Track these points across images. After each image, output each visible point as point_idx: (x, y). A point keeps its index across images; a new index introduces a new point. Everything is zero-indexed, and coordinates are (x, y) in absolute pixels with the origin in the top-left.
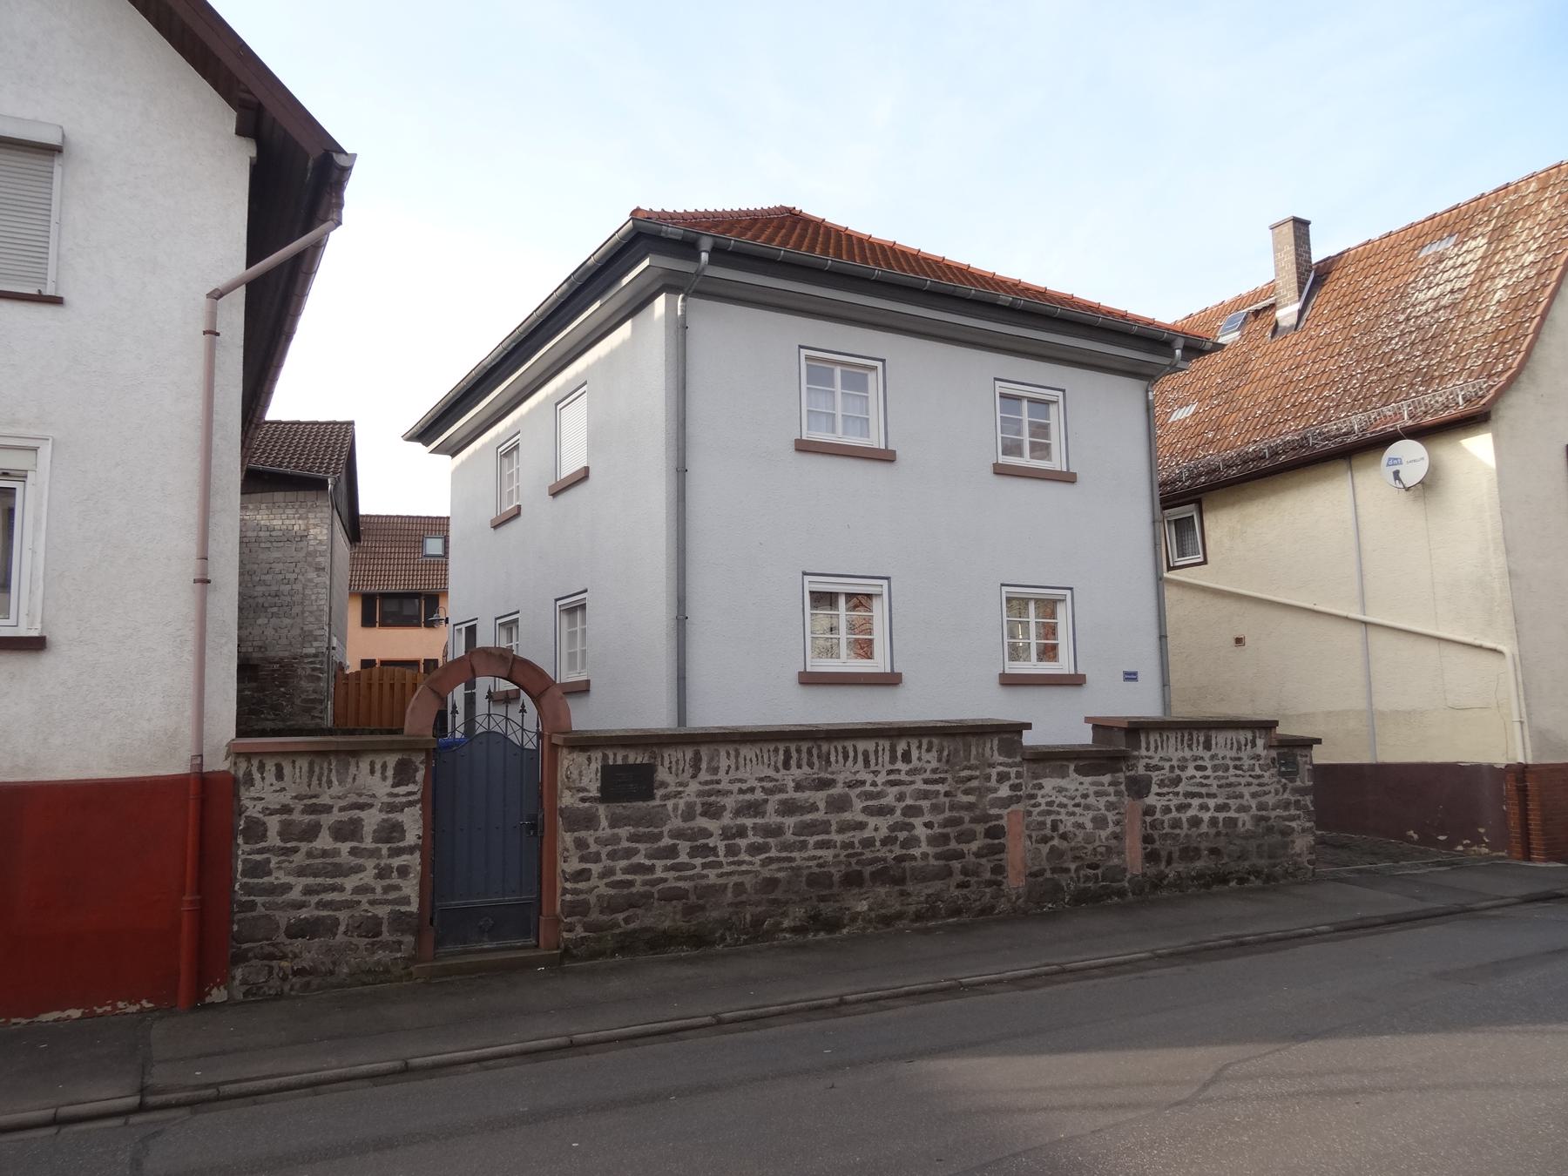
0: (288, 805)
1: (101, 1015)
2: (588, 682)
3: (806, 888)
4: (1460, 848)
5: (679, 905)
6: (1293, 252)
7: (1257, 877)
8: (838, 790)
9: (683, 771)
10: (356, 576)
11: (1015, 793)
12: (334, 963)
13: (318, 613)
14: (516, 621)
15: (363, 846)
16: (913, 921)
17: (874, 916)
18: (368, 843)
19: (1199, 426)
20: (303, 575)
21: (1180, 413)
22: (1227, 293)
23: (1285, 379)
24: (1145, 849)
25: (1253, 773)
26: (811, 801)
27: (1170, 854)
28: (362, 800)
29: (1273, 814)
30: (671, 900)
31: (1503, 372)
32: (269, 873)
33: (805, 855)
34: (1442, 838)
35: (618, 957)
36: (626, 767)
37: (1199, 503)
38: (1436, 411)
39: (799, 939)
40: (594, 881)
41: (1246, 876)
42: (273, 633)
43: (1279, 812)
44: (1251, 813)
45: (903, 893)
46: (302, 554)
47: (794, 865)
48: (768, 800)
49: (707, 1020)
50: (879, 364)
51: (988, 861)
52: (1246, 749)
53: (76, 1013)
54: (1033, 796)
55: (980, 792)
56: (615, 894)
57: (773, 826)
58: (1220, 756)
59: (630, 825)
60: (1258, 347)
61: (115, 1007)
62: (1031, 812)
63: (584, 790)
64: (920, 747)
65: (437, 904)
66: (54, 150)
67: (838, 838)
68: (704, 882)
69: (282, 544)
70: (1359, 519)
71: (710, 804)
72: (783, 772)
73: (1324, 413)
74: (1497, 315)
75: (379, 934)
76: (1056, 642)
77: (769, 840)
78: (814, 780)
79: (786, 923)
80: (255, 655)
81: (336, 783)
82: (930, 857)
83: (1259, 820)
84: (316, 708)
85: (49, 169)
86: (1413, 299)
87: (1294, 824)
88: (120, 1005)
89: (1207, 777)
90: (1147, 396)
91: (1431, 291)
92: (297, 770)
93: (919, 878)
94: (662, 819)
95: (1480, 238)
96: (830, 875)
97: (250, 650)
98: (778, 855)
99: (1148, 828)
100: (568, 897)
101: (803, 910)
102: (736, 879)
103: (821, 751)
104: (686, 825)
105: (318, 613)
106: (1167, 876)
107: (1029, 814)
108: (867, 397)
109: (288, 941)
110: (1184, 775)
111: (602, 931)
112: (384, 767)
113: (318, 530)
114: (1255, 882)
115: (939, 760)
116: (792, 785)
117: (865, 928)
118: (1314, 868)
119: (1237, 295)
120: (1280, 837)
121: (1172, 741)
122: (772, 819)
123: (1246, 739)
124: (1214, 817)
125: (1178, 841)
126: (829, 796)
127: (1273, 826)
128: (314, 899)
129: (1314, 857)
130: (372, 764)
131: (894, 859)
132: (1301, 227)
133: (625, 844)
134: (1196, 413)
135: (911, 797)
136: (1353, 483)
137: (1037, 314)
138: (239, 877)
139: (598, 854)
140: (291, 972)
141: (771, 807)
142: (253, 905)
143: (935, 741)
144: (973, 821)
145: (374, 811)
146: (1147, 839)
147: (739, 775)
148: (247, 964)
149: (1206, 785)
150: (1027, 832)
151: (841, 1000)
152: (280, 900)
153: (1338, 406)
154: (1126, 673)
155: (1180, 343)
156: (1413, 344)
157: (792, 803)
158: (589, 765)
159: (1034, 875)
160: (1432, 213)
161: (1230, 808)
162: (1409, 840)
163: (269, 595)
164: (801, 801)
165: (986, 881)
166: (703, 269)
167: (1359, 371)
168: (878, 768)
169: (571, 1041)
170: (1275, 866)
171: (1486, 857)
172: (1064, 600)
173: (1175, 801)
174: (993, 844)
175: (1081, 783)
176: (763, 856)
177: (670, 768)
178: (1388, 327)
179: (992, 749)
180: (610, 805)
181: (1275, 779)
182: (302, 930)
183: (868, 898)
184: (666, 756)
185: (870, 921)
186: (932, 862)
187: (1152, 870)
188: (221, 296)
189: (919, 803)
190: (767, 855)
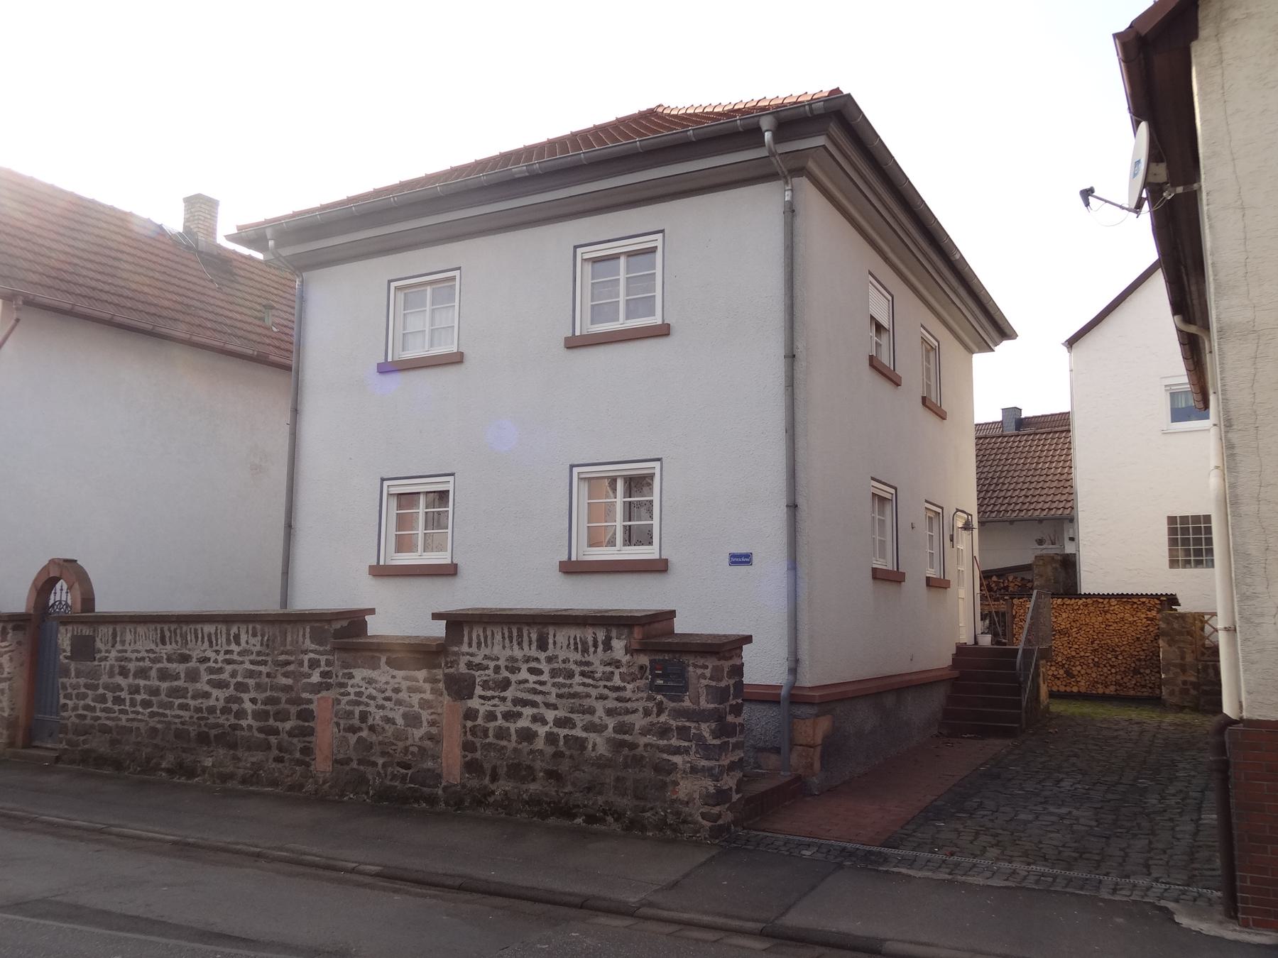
5: (108, 736)
7: (616, 820)
8: (193, 664)
11: (325, 680)
24: (465, 756)
25: (608, 684)
27: (494, 768)
43: (649, 739)
47: (166, 719)
58: (560, 659)
67: (192, 703)
72: (161, 646)
77: (153, 698)
79: (164, 765)
83: (618, 745)
87: (677, 759)
89: (542, 683)
96: (188, 732)
106: (493, 792)
107: (339, 702)
110: (513, 678)
115: (262, 645)
121: (498, 637)
125: (504, 754)
127: (642, 757)
143: (258, 627)
144: (288, 701)
146: (468, 747)
149: (541, 693)
150: (335, 720)
159: (336, 761)
170: (644, 811)
174: (304, 726)
175: (393, 677)
181: (644, 695)
187: (474, 783)
189: (247, 680)
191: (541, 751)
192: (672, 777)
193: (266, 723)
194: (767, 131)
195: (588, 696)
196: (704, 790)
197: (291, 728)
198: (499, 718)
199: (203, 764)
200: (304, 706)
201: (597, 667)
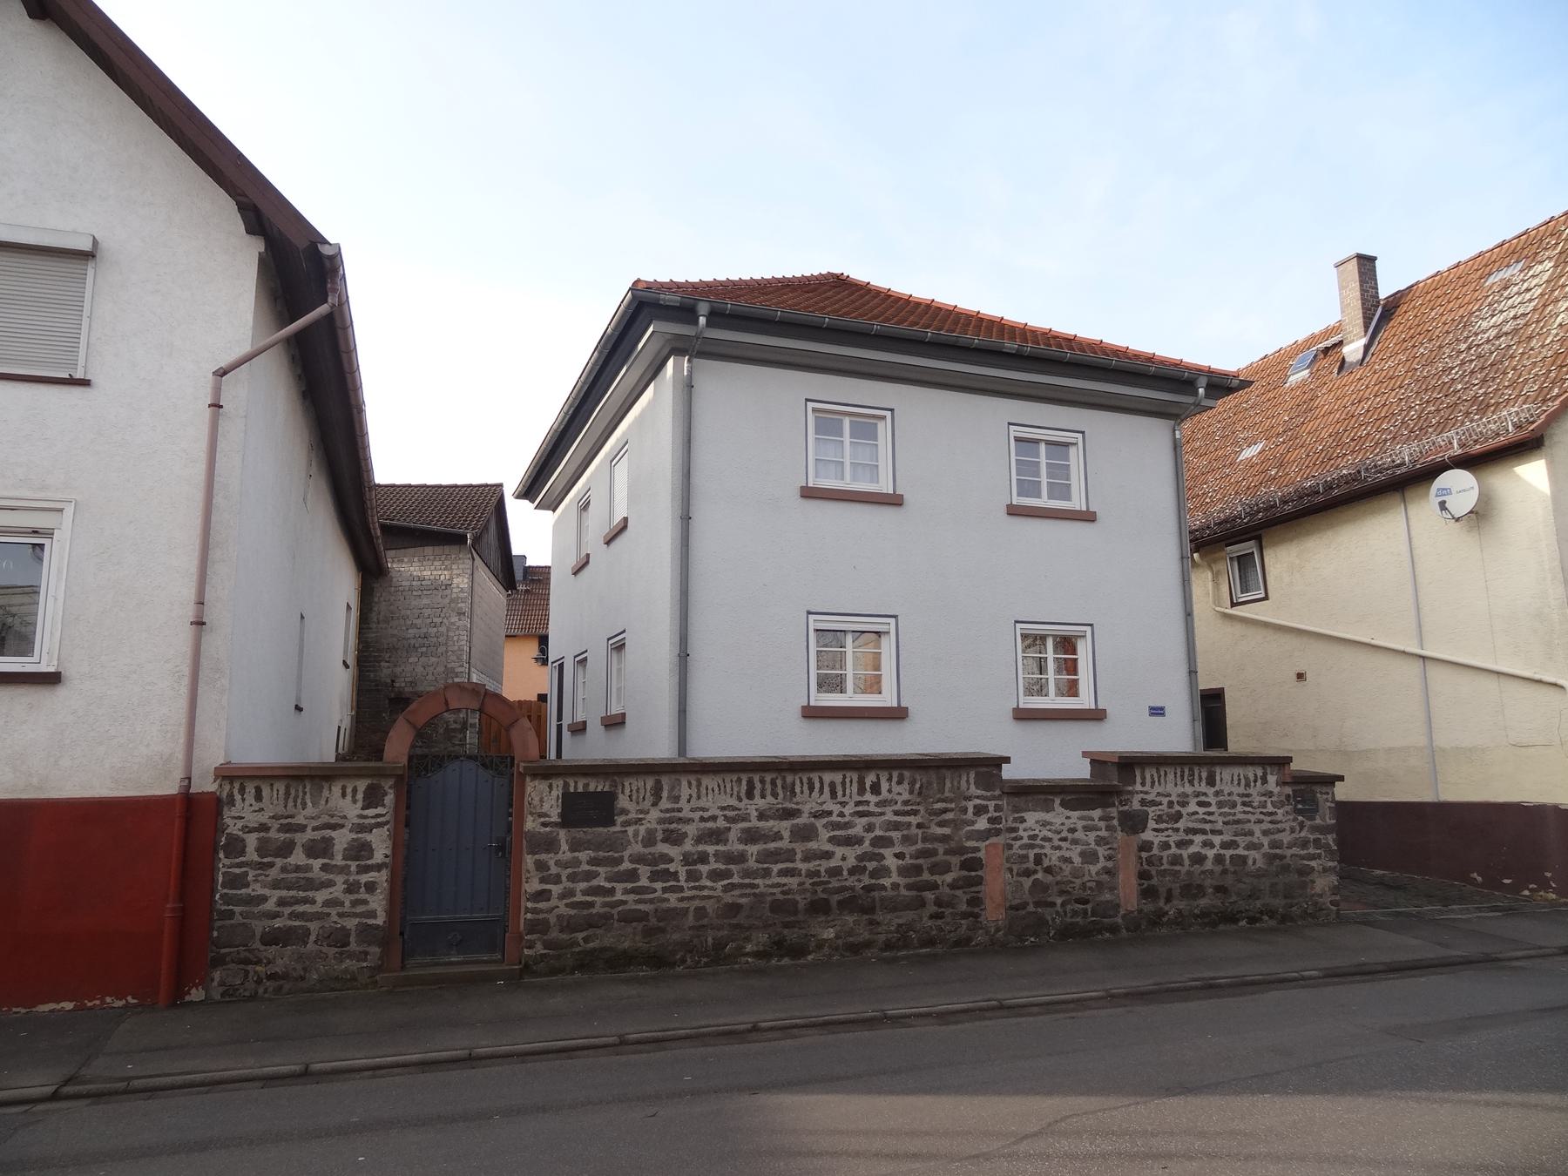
0: (265, 824)
1: (91, 1008)
3: (769, 914)
4: (1526, 893)
5: (639, 926)
6: (1358, 288)
7: (1271, 917)
8: (803, 820)
9: (644, 798)
12: (305, 969)
15: (334, 863)
16: (882, 950)
17: (841, 944)
18: (338, 860)
21: (1248, 452)
25: (1264, 811)
26: (775, 830)
27: (1169, 891)
28: (333, 821)
29: (1289, 852)
30: (632, 922)
31: (1558, 396)
32: (247, 885)
33: (768, 882)
34: (1507, 881)
35: (577, 975)
36: (586, 795)
37: (1259, 539)
38: (1487, 440)
39: (762, 963)
40: (554, 902)
41: (1258, 915)
43: (1295, 850)
44: (1263, 851)
45: (871, 923)
46: (447, 600)
47: (757, 891)
48: (730, 828)
49: (611, 1040)
50: (888, 414)
52: (1255, 786)
53: (69, 1006)
54: (1015, 830)
55: (956, 824)
56: (575, 914)
58: (1226, 793)
61: (103, 1002)
62: (1012, 845)
63: (546, 815)
64: (890, 780)
65: (408, 918)
66: (88, 256)
67: (803, 867)
68: (665, 905)
69: (429, 592)
70: (1414, 552)
71: (672, 831)
72: (746, 801)
73: (1381, 445)
74: (1558, 338)
75: (348, 944)
76: (879, 673)
78: (778, 810)
79: (749, 948)
80: (407, 689)
81: (309, 804)
82: (902, 888)
83: (1271, 858)
84: (456, 737)
85: (84, 272)
86: (1476, 327)
87: (1313, 863)
88: (108, 1000)
90: (1174, 434)
91: (1495, 318)
92: (275, 792)
94: (622, 844)
95: (1547, 261)
96: (795, 903)
97: (403, 685)
98: (741, 881)
100: (529, 916)
102: (697, 903)
103: (785, 781)
104: (647, 851)
106: (1167, 913)
107: (1010, 847)
108: (877, 445)
109: (262, 948)
110: (1184, 811)
111: (562, 949)
112: (355, 791)
113: (460, 580)
115: (911, 792)
117: (831, 956)
118: (1338, 910)
120: (1296, 876)
121: (1171, 776)
126: (793, 825)
128: (287, 910)
130: (344, 789)
131: (862, 888)
132: (1366, 263)
133: (586, 867)
134: (1263, 451)
136: (1406, 513)
138: (219, 888)
139: (558, 876)
140: (264, 977)
141: (733, 835)
142: (231, 914)
143: (907, 774)
145: (344, 831)
146: (1143, 875)
147: (701, 803)
148: (224, 967)
149: (1210, 822)
150: (1008, 865)
151: (754, 1027)
152: (256, 910)
153: (1394, 438)
154: (1151, 708)
155: (1203, 381)
156: (1472, 372)
157: (755, 832)
159: (1012, 908)
160: (1500, 241)
161: (1238, 846)
162: (1473, 882)
164: (764, 830)
166: (701, 332)
167: (1418, 402)
168: (846, 799)
169: (470, 1054)
171: (1552, 903)
172: (1084, 636)
173: (1175, 838)
175: (1068, 818)
176: (726, 882)
178: (1450, 356)
179: (968, 783)
181: (1291, 817)
182: (275, 938)
184: (627, 784)
185: (837, 949)
186: (904, 892)
187: (1149, 907)
188: (225, 373)
190: (729, 881)
192: (1310, 877)
193: (920, 878)
195: (1249, 821)
199: (819, 938)
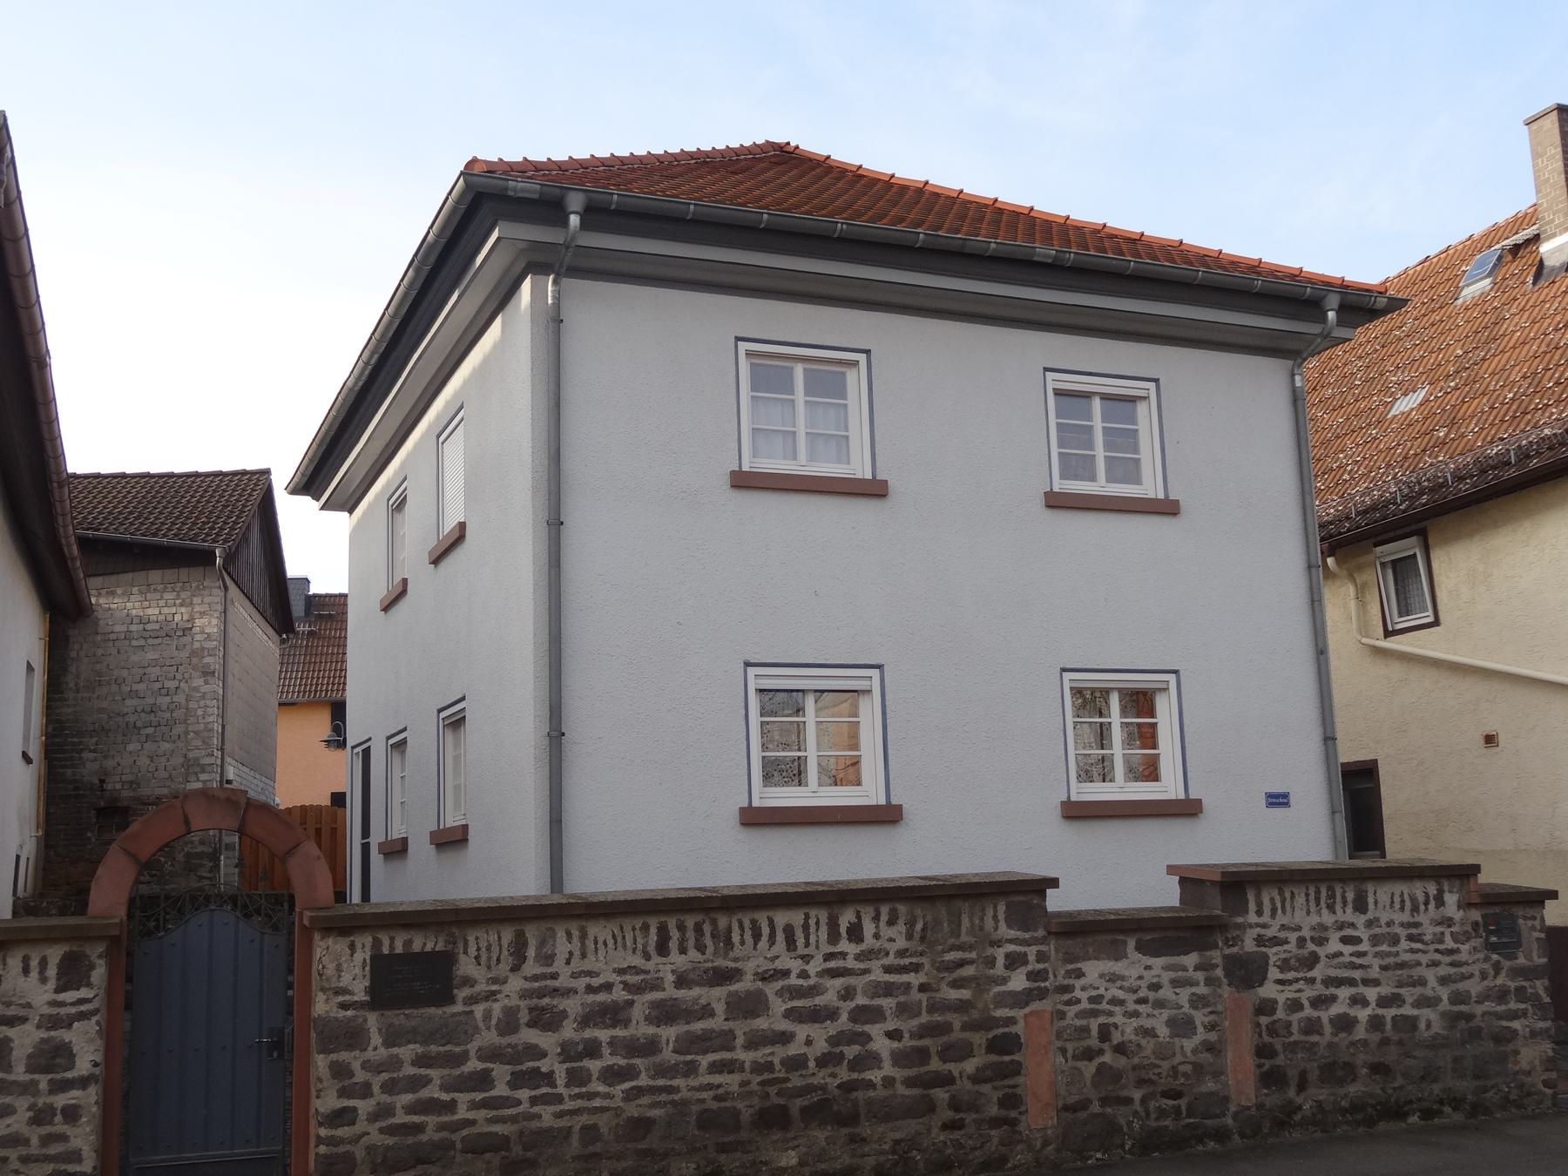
2: (465, 828)
5: (495, 1159)
7: (1455, 1109)
9: (498, 960)
10: (323, 678)
11: (1037, 984)
13: (206, 734)
14: (404, 741)
18: (19, 1073)
19: (1429, 421)
20: (186, 682)
22: (1477, 224)
23: (1548, 346)
24: (1260, 1066)
26: (703, 1002)
29: (1479, 1010)
30: (483, 1153)
36: (409, 958)
37: (1423, 534)
40: (361, 1126)
42: (148, 763)
43: (1489, 1006)
46: (185, 654)
47: (676, 1097)
50: (862, 358)
51: (995, 1088)
54: (1068, 989)
55: (980, 984)
57: (642, 1040)
58: (1383, 922)
59: (415, 1043)
60: (1515, 299)
64: (876, 918)
68: (535, 1125)
71: (543, 1009)
72: (656, 959)
77: (637, 1061)
80: (125, 794)
83: (1452, 1019)
87: (1516, 1025)
90: (1293, 381)
93: (878, 1116)
94: (466, 1033)
96: (735, 1113)
97: (118, 786)
98: (651, 1083)
99: (1264, 1034)
100: (322, 1149)
101: (694, 1166)
102: (584, 1119)
105: (206, 734)
106: (1300, 1108)
107: (1061, 1015)
110: (1321, 952)
112: (43, 963)
113: (205, 620)
114: (1452, 1116)
115: (909, 937)
116: (671, 978)
119: (1492, 224)
122: (640, 1028)
123: (1427, 895)
124: (1376, 1016)
125: (1316, 1053)
126: (730, 994)
127: (1480, 1029)
129: (1554, 1075)
130: (26, 961)
131: (838, 1087)
133: (409, 1070)
134: (1426, 401)
135: (864, 993)
137: (1107, 273)
141: (638, 1012)
143: (902, 909)
145: (28, 1027)
146: (1263, 1051)
147: (588, 965)
149: (1361, 966)
150: (1059, 1044)
154: (1269, 796)
155: (1333, 301)
157: (672, 1006)
158: (352, 956)
161: (1404, 1002)
163: (143, 711)
165: (991, 1118)
168: (811, 950)
170: (1485, 1090)
173: (1309, 993)
175: (1148, 968)
177: (477, 958)
179: (996, 919)
180: (386, 1013)
181: (1481, 956)
183: (798, 1146)
184: (471, 939)
186: (901, 1090)
187: (1273, 1099)
191: (1365, 1043)
192: (1511, 1047)
194: (1332, 310)
195: (1419, 964)
196: (1543, 1054)
197: (977, 1069)
198: (1305, 1006)
200: (1002, 1030)
201: (1426, 928)
